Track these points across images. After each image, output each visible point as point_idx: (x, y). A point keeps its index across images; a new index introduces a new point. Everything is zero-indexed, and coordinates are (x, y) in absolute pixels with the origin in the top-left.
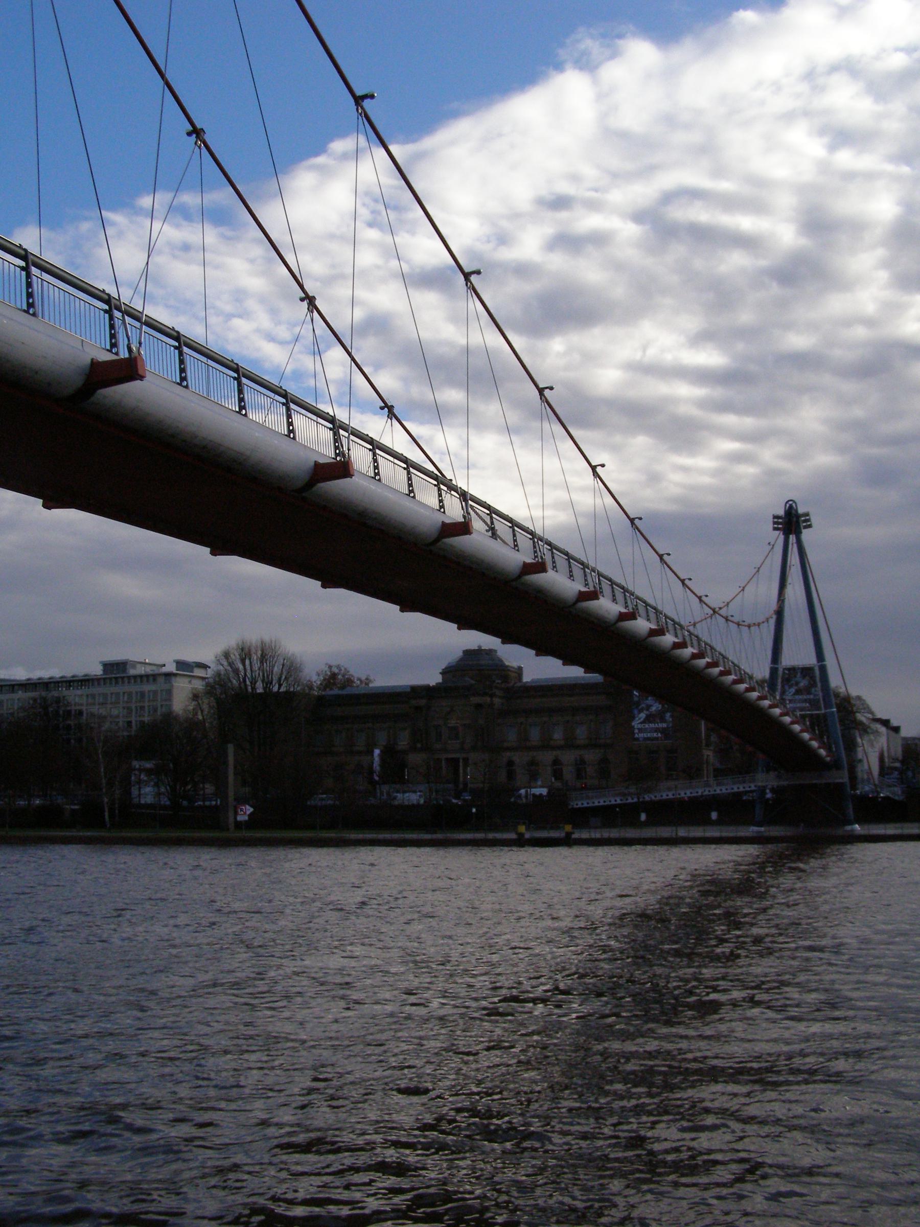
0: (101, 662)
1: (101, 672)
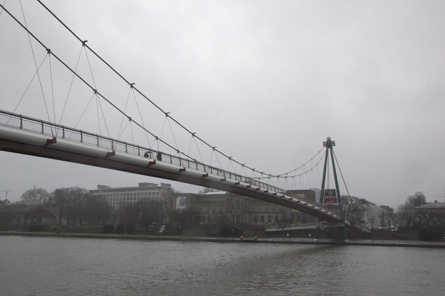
0: (138, 183)
1: (138, 186)
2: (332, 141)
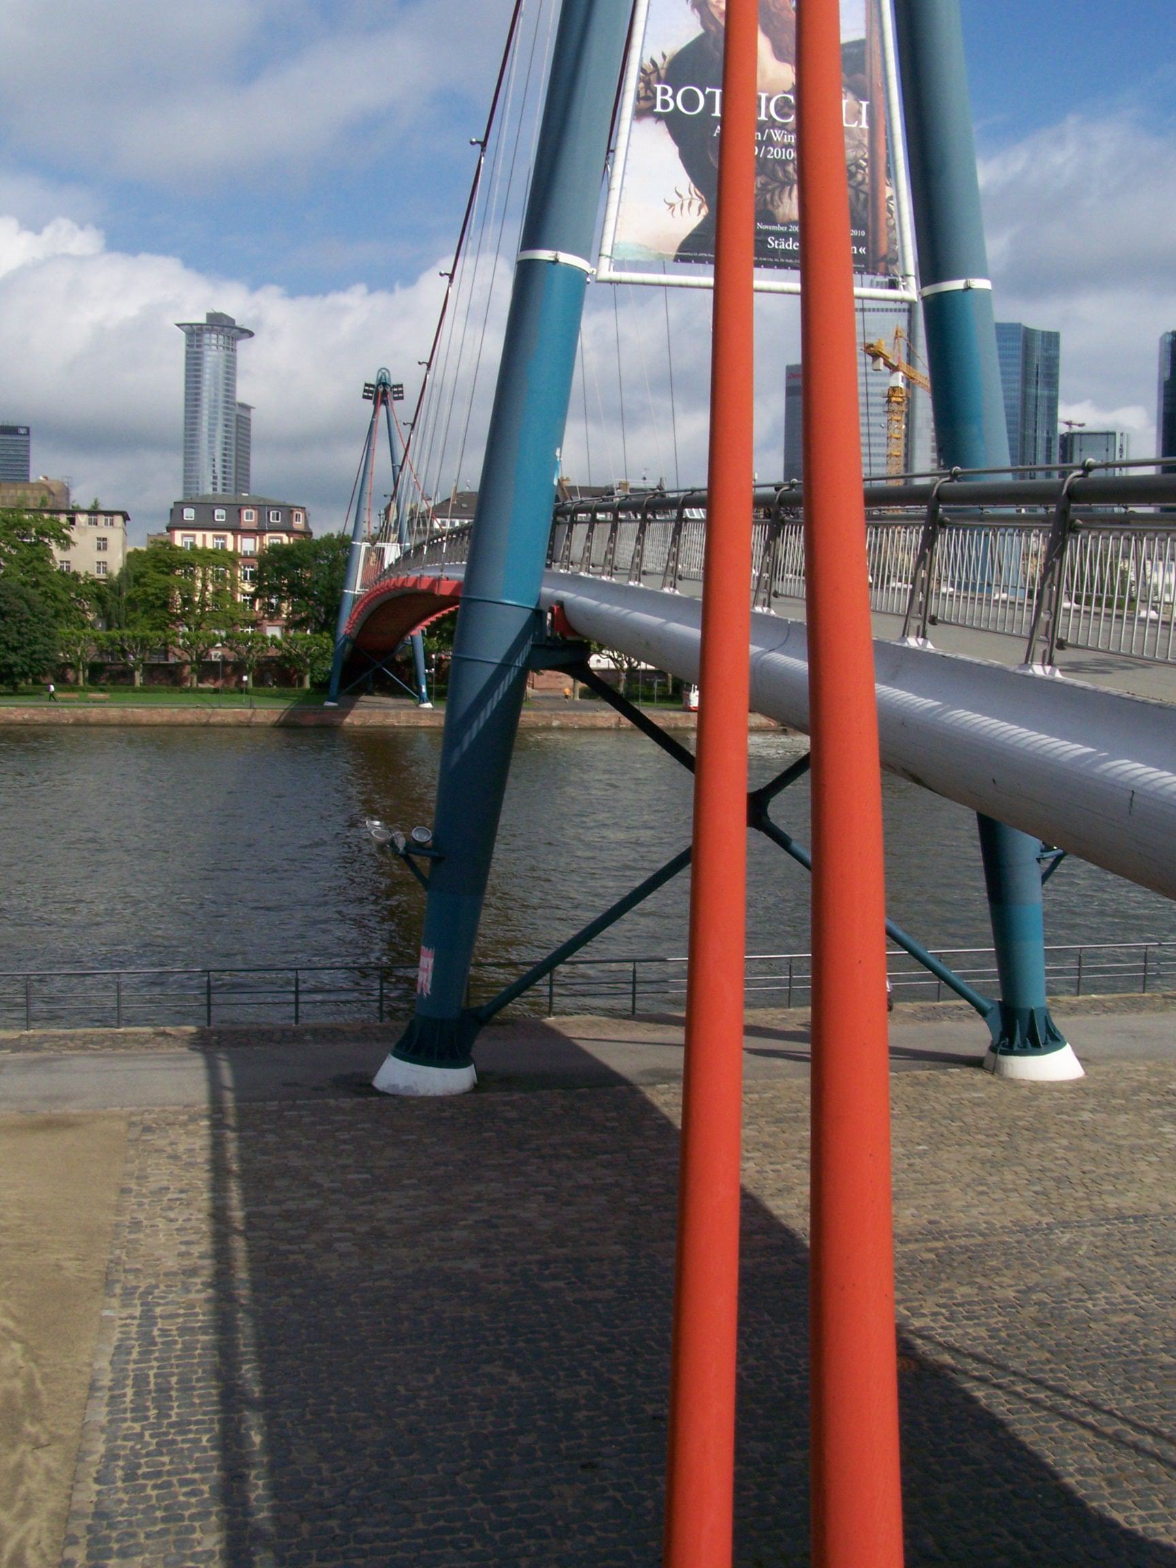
2: (394, 382)
